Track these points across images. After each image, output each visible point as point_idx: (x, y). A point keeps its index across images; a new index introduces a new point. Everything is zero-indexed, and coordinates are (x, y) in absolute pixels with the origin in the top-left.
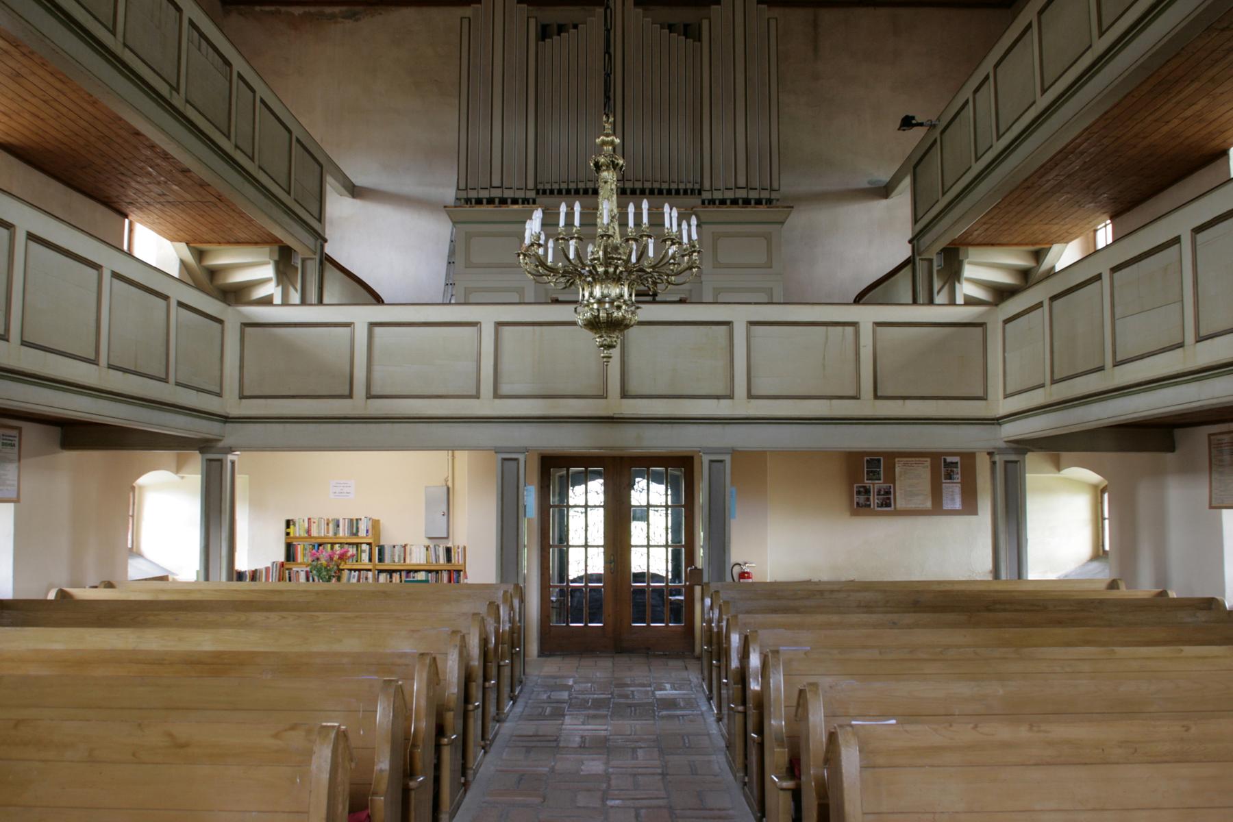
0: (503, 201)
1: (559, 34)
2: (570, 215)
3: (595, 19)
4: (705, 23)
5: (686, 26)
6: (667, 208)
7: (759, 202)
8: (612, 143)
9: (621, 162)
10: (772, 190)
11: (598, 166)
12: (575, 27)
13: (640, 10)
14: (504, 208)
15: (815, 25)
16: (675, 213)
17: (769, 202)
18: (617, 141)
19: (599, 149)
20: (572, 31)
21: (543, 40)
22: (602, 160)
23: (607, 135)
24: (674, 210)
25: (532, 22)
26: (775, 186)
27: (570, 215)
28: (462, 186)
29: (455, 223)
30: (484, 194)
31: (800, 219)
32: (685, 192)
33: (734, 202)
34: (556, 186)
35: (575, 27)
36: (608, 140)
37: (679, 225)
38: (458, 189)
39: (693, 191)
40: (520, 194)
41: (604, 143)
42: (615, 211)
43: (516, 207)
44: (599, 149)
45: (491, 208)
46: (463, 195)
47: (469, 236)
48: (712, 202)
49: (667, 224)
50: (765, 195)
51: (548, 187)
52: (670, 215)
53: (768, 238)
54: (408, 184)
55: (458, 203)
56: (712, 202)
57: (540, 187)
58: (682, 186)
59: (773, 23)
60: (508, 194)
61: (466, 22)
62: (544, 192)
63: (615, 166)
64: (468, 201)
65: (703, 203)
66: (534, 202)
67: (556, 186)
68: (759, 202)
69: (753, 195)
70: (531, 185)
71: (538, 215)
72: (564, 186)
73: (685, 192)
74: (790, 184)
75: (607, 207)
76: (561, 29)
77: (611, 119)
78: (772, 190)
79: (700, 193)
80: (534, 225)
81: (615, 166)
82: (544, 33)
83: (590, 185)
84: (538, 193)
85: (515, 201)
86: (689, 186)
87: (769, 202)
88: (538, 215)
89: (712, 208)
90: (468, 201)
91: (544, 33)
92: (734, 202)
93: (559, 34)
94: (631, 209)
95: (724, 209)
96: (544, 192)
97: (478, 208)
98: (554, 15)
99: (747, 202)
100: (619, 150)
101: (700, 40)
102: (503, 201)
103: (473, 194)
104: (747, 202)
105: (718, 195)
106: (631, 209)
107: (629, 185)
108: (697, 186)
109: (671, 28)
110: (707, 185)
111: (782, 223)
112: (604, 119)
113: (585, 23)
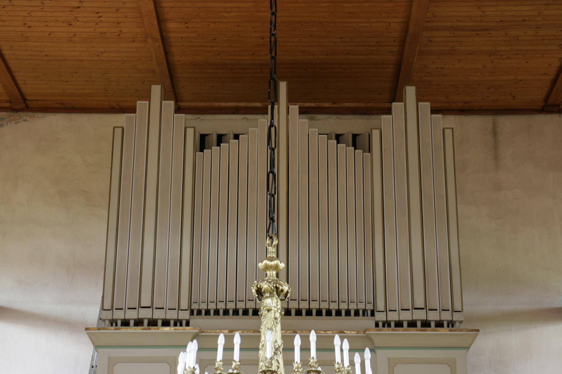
0: (153, 323)
1: (218, 145)
2: (229, 348)
3: (256, 128)
4: (376, 134)
5: (355, 136)
6: (337, 340)
7: (439, 324)
8: (276, 267)
9: (286, 288)
10: (454, 311)
11: (260, 292)
12: (236, 137)
13: (305, 120)
14: (153, 330)
15: (495, 134)
16: (346, 345)
17: (451, 324)
18: (282, 265)
19: (262, 274)
20: (233, 142)
21: (202, 150)
22: (265, 286)
23: (271, 259)
24: (346, 341)
25: (190, 132)
26: (458, 307)
27: (229, 348)
28: (107, 305)
29: (96, 347)
30: (132, 315)
31: (487, 342)
32: (357, 313)
33: (412, 324)
34: (212, 307)
35: (236, 137)
36: (271, 264)
37: (352, 363)
38: (103, 309)
39: (364, 311)
40: (172, 315)
41: (267, 268)
42: (280, 342)
43: (166, 329)
44: (262, 274)
45: (139, 329)
46: (108, 315)
47: (112, 362)
48: (386, 324)
49: (338, 359)
50: (446, 316)
51: (203, 307)
52: (341, 347)
53: (452, 365)
54: (45, 302)
55: (102, 325)
56: (386, 324)
57: (195, 307)
58: (353, 307)
59: (448, 132)
60: (159, 315)
61: (118, 132)
62: (199, 312)
63: (279, 292)
64: (113, 322)
65: (377, 325)
66: (188, 324)
67: (212, 307)
68: (439, 324)
69: (433, 317)
70: (184, 304)
71: (193, 346)
72: (221, 306)
73: (357, 313)
74: (473, 302)
75: (271, 337)
76: (220, 139)
77: (275, 242)
78: (454, 311)
79: (373, 314)
80: (188, 358)
81: (279, 292)
82: (203, 143)
83: (251, 305)
84: (192, 313)
85: (166, 323)
86: (361, 306)
87: (451, 324)
88: (193, 346)
89: (386, 331)
90: (113, 322)
91: (203, 143)
92: (412, 324)
93: (218, 145)
94: (297, 341)
95: (400, 331)
96: (199, 312)
97: (124, 330)
98: (213, 124)
99: (426, 324)
100: (283, 275)
101: (370, 151)
102: (153, 323)
103: (119, 315)
104: (426, 324)
105: (393, 317)
106: (297, 341)
107: (293, 305)
108: (370, 307)
109: (338, 138)
110: (380, 305)
111: (468, 348)
112: (268, 242)
113: (247, 133)
